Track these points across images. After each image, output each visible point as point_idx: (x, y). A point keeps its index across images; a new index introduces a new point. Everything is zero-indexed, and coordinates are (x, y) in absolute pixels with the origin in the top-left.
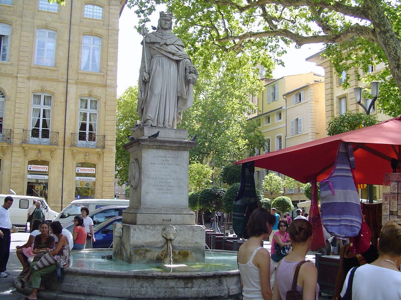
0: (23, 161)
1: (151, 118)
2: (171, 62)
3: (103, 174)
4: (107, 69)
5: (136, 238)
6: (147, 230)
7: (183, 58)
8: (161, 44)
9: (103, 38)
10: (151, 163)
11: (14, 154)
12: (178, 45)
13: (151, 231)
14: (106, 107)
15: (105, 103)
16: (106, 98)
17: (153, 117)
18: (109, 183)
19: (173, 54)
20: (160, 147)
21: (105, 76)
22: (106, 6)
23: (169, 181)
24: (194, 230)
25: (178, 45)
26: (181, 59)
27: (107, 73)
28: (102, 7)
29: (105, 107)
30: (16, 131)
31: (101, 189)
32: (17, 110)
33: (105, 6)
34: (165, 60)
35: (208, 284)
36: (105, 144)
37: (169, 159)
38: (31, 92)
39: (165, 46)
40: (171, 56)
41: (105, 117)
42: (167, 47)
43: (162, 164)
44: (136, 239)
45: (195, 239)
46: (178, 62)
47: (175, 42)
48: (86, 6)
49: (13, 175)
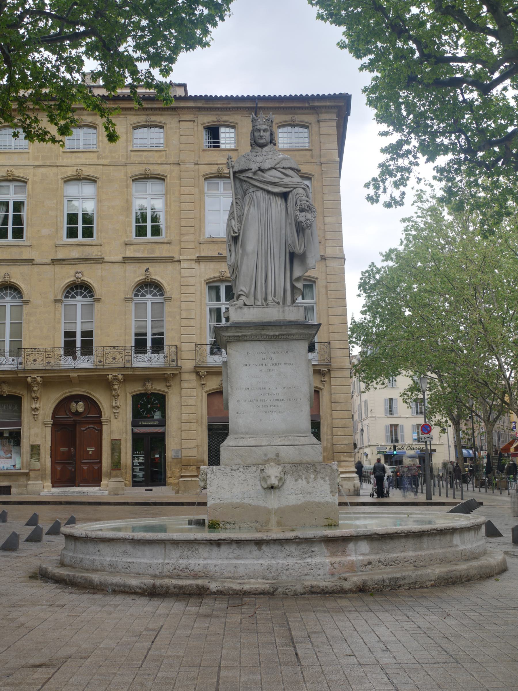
1: (245, 293)
3: (331, 406)
5: (217, 486)
6: (234, 473)
7: (292, 189)
10: (244, 365)
12: (284, 168)
13: (240, 474)
14: (328, 294)
15: (326, 287)
16: (326, 278)
18: (343, 422)
19: (274, 184)
22: (313, 125)
23: (274, 392)
24: (317, 470)
25: (284, 168)
26: (288, 190)
27: (324, 237)
29: (327, 294)
30: (185, 347)
31: (329, 432)
32: (184, 314)
34: (261, 195)
35: (288, 553)
36: (331, 356)
38: (203, 282)
40: (270, 188)
41: (328, 310)
44: (217, 488)
46: (285, 196)
49: (184, 418)
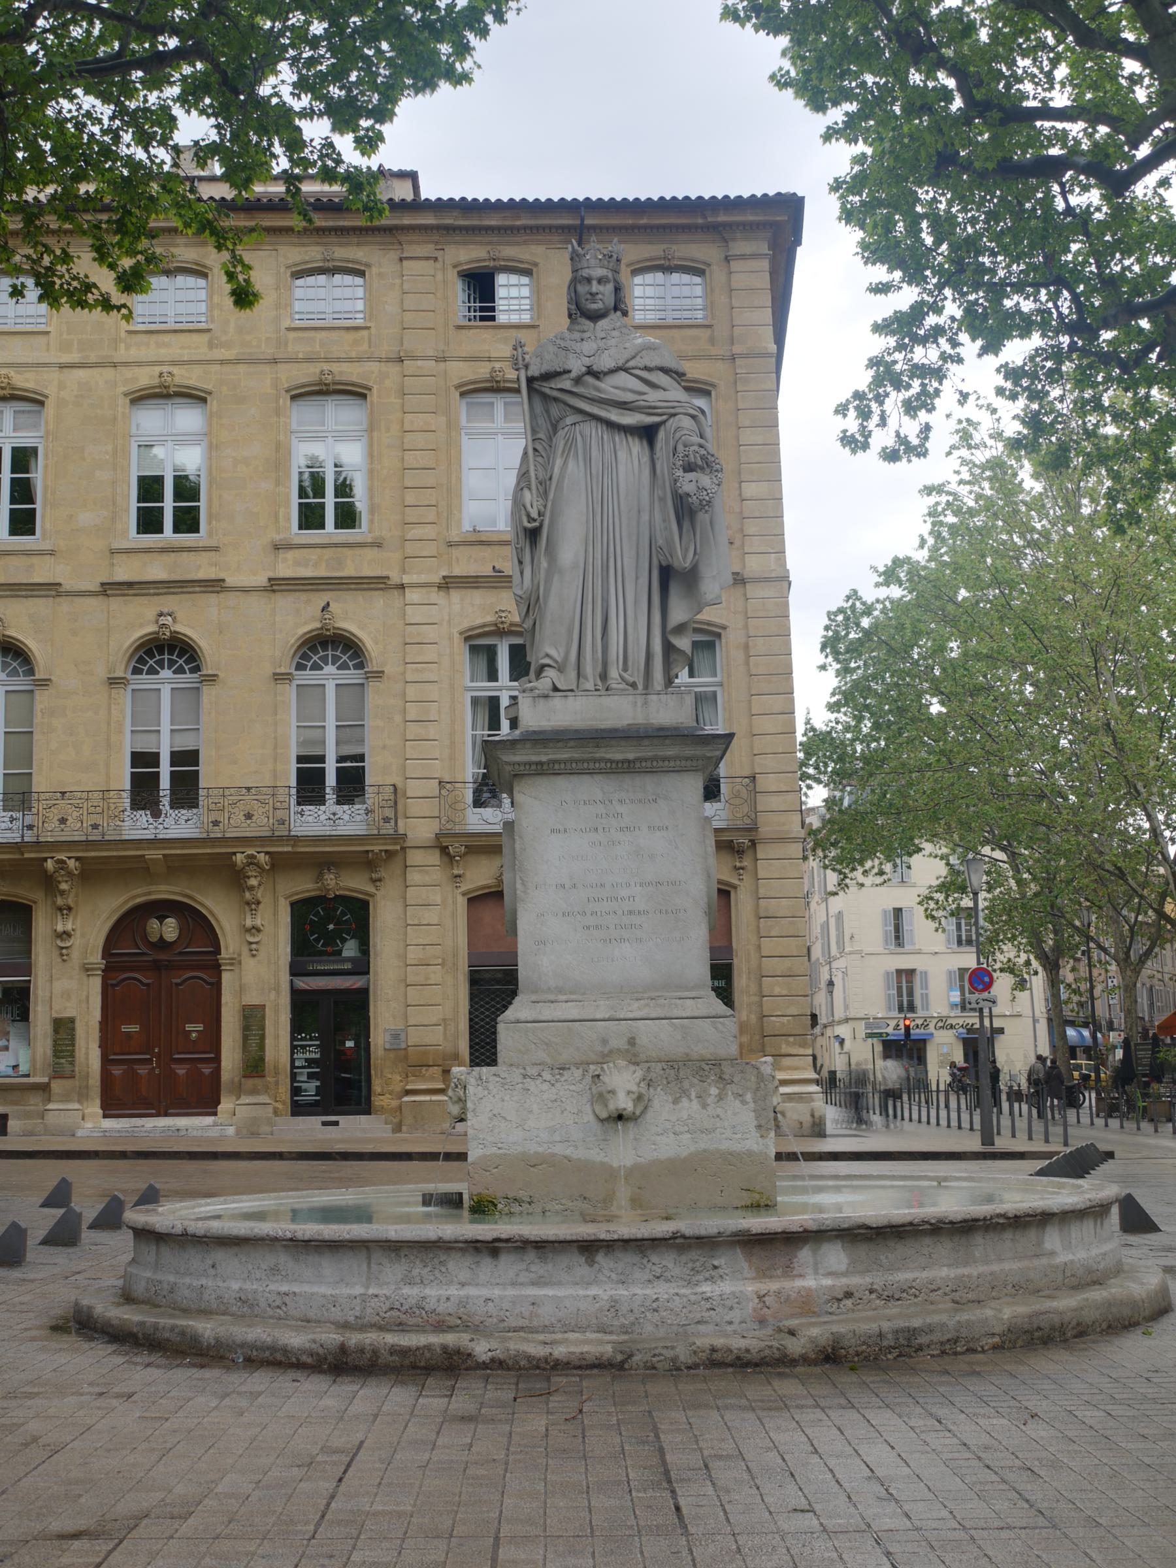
0: (450, 901)
1: (556, 662)
2: (617, 439)
3: (758, 927)
4: (741, 512)
5: (490, 1115)
6: (530, 1083)
7: (664, 417)
8: (573, 375)
9: (713, 393)
10: (553, 831)
11: (414, 877)
12: (646, 368)
13: (545, 1086)
15: (746, 647)
16: (746, 626)
17: (562, 655)
18: (787, 963)
19: (623, 406)
20: (629, 767)
21: (738, 542)
22: (714, 267)
23: (625, 893)
25: (646, 368)
26: (657, 419)
27: (742, 530)
28: (699, 272)
29: (747, 663)
30: (414, 788)
31: (753, 988)
32: (413, 712)
33: (709, 265)
34: (592, 430)
36: (759, 808)
37: (620, 809)
38: (456, 635)
39: (590, 379)
40: (614, 416)
41: (750, 702)
42: (597, 383)
43: (596, 830)
44: (490, 1119)
45: (729, 1113)
46: (648, 434)
47: (634, 357)
48: (638, 280)
49: (413, 954)
